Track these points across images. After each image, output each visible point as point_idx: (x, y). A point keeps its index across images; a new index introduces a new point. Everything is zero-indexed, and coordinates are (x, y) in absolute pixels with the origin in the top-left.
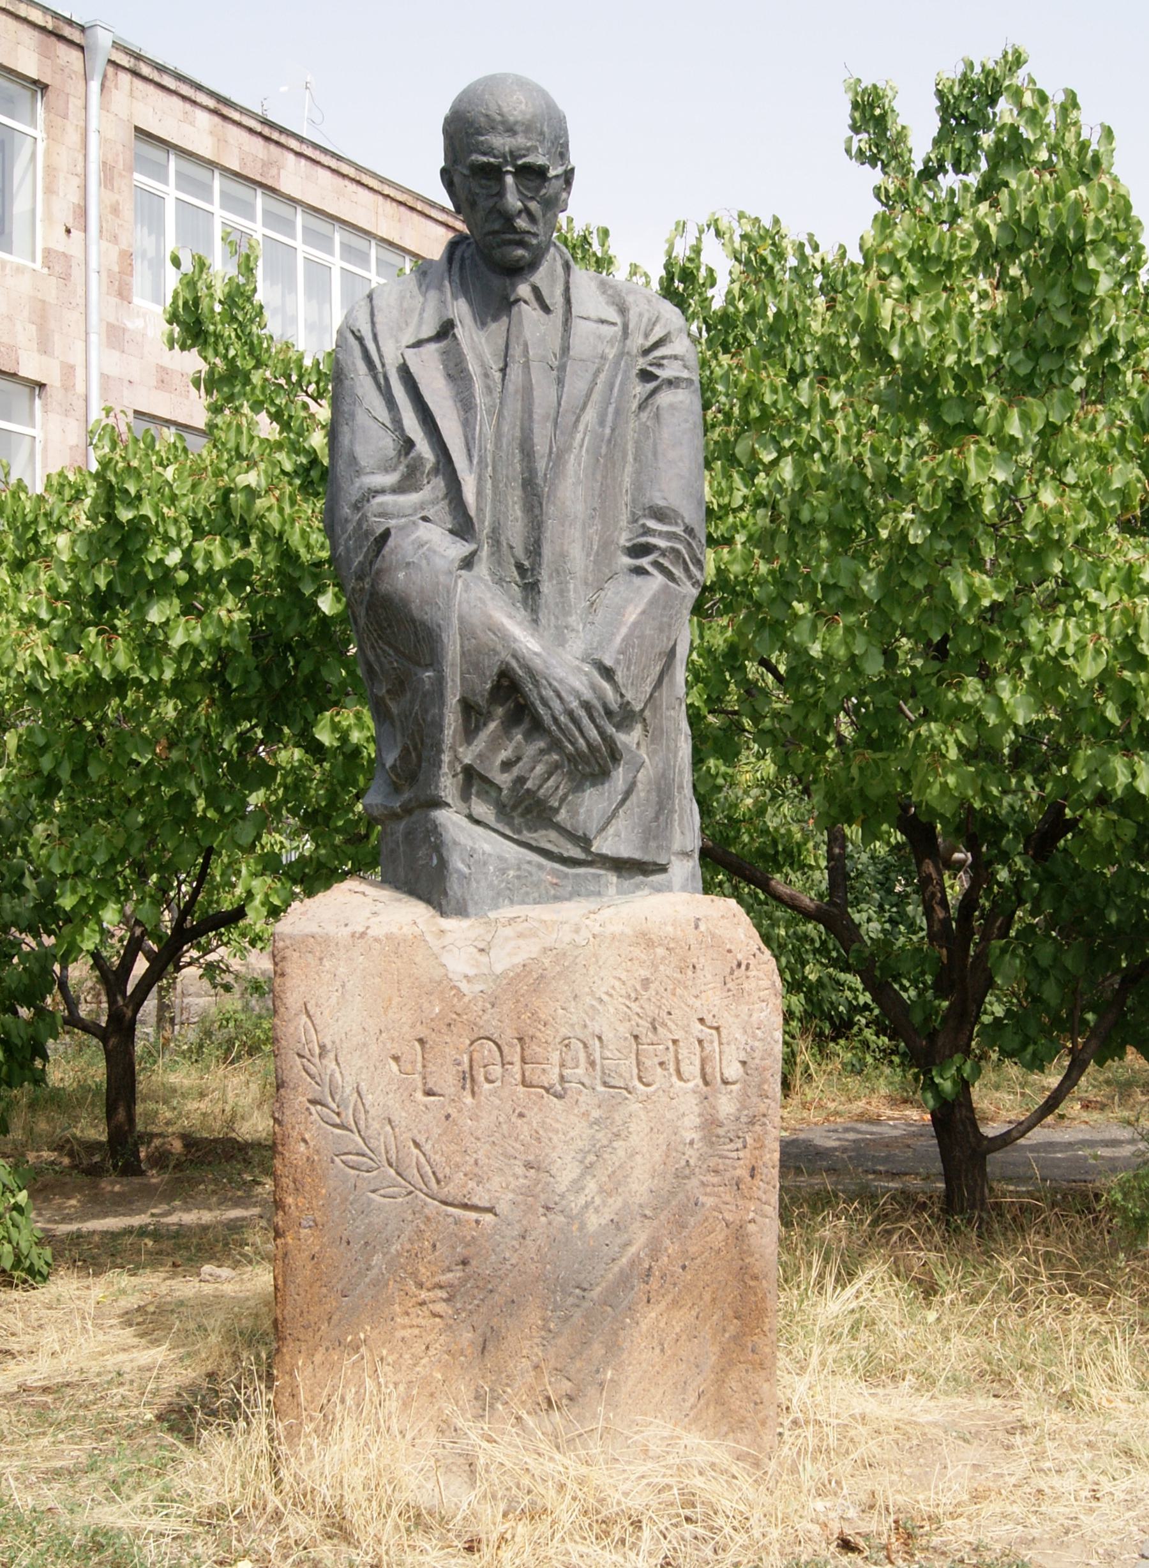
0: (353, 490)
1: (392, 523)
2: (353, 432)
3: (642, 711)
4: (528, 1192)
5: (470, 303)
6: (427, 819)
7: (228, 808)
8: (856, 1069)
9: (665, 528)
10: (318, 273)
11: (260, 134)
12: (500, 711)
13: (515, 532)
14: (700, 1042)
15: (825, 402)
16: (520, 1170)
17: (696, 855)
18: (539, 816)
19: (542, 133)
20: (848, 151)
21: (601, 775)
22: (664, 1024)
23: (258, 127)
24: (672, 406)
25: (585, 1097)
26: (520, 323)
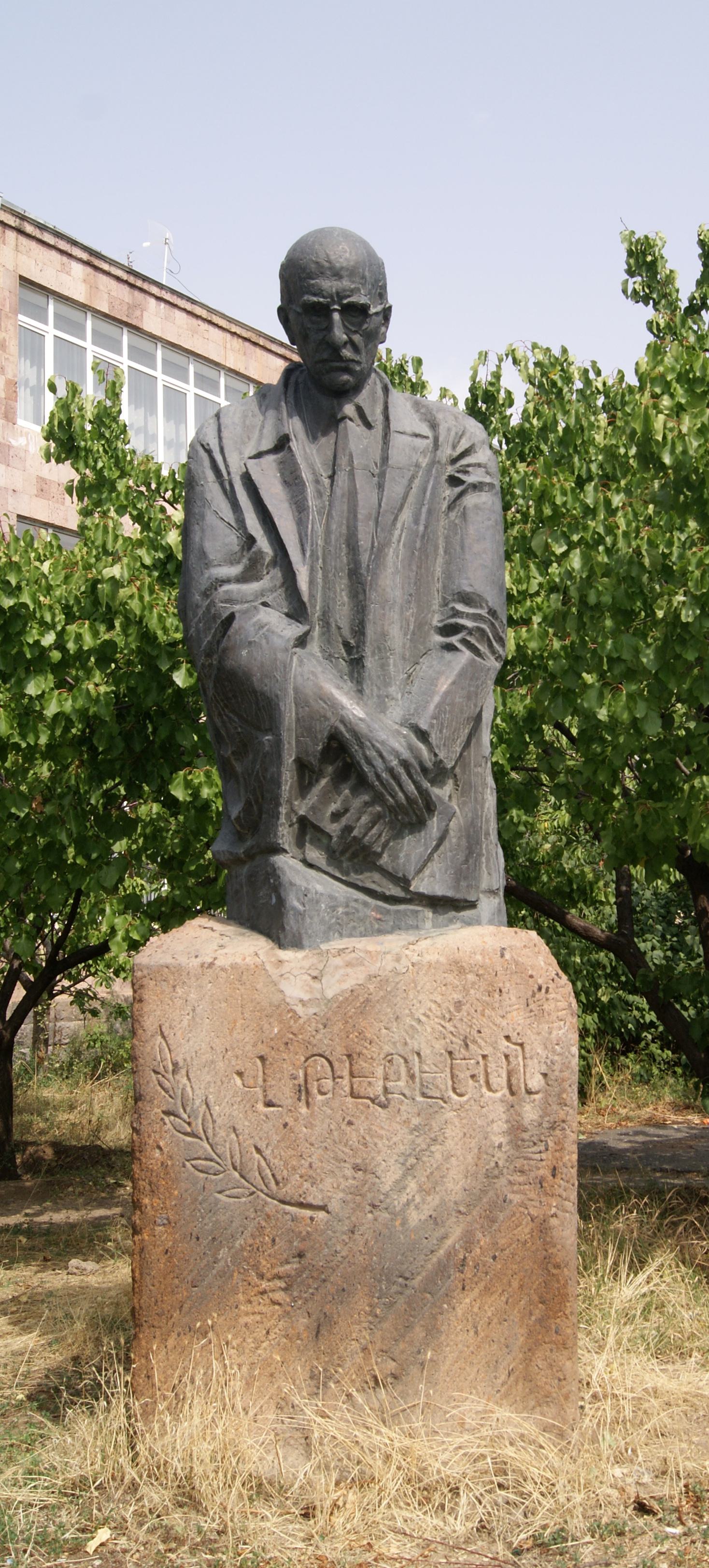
0: (203, 581)
1: (237, 608)
2: (203, 531)
3: (453, 768)
4: (356, 1192)
5: (303, 420)
7: (94, 856)
8: (644, 1079)
9: (471, 611)
10: (175, 399)
11: (126, 282)
12: (330, 769)
13: (342, 615)
14: (507, 1057)
15: (608, 502)
16: (349, 1172)
17: (501, 893)
19: (363, 277)
20: (625, 291)
21: (418, 825)
22: (475, 1042)
23: (125, 276)
24: (477, 507)
25: (406, 1107)
26: (346, 436)
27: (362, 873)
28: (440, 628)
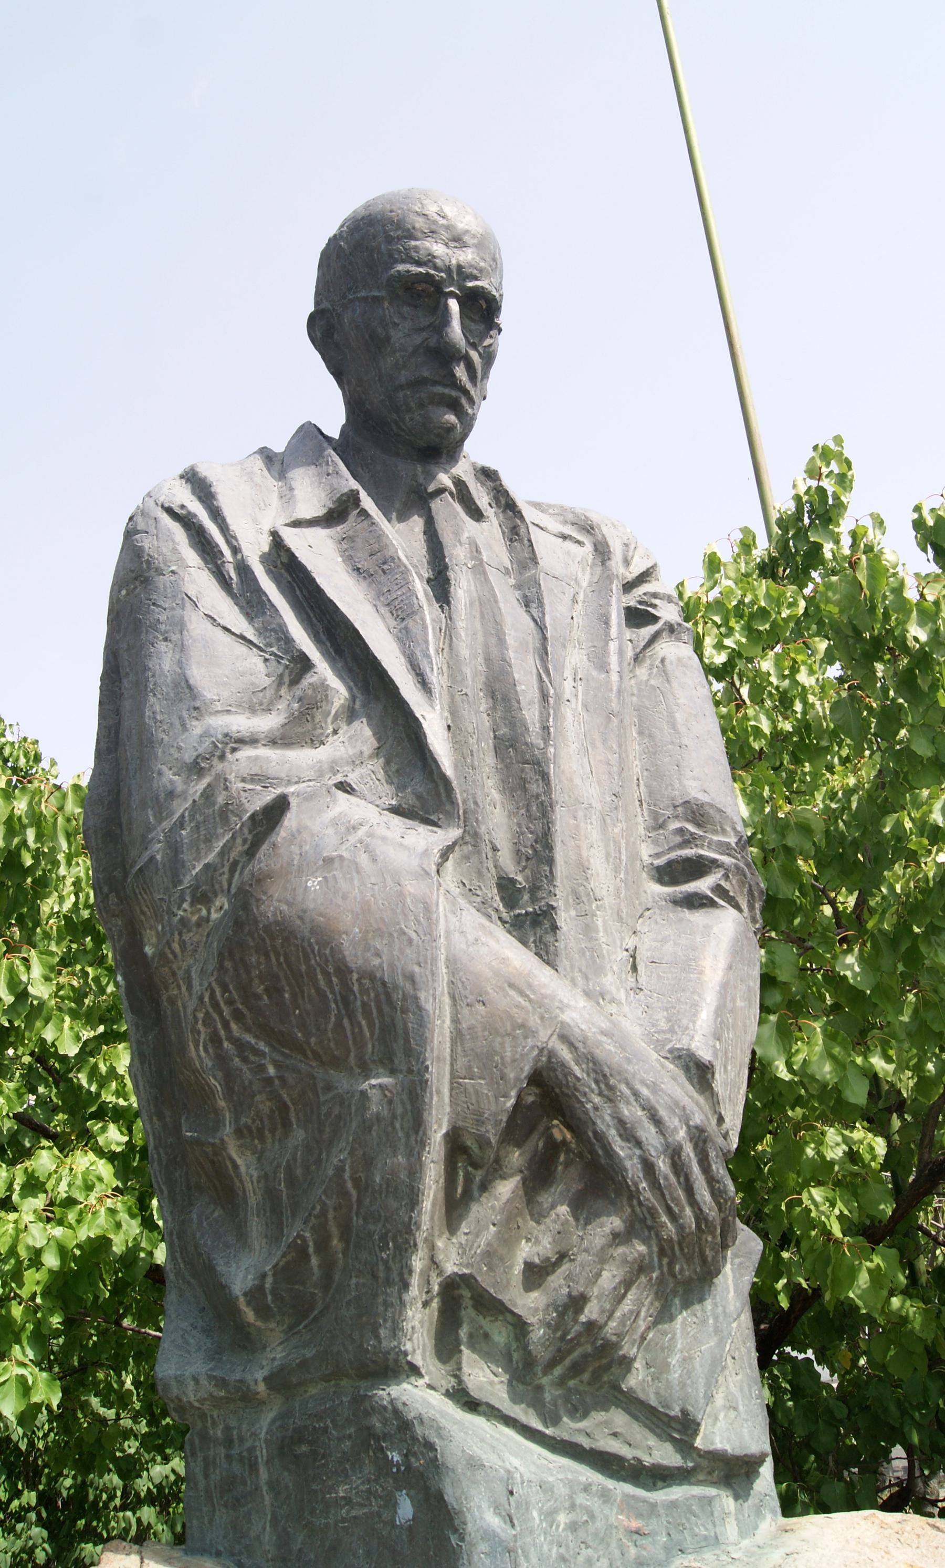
1: (292, 789)
6: (362, 1405)
12: (516, 1157)
18: (596, 1377)
27: (585, 1415)
28: (658, 869)
